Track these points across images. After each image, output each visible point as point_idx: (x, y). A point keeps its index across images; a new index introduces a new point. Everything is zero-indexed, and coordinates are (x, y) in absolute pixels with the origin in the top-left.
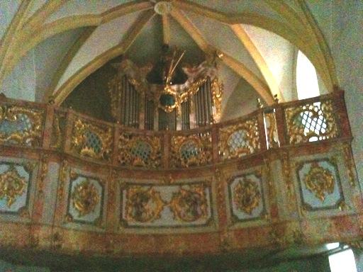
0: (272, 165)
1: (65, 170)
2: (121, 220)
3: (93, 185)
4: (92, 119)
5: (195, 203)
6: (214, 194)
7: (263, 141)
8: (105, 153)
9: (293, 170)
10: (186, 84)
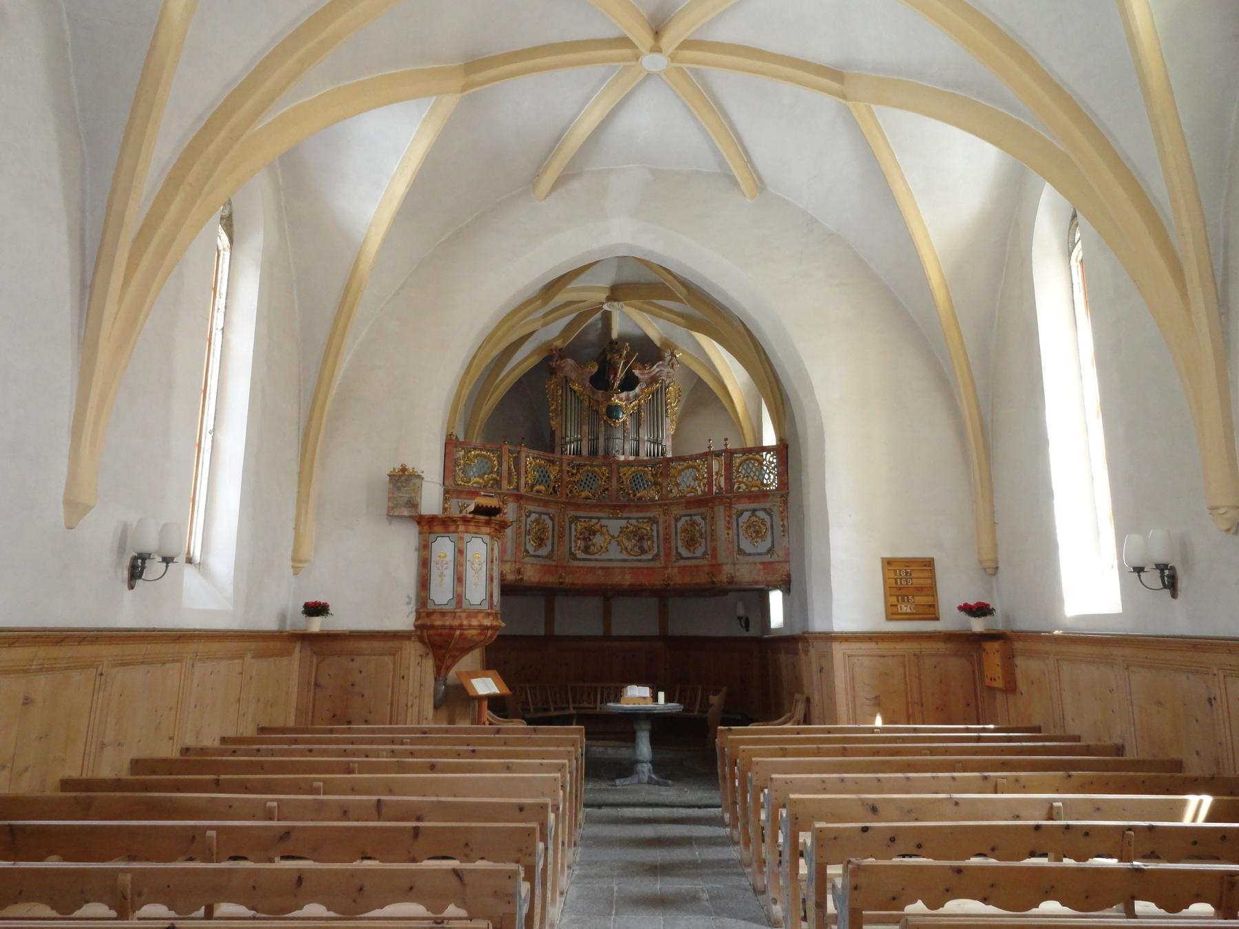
2: (571, 553)
5: (641, 539)
6: (661, 532)
7: (710, 484)
9: (734, 517)
10: (637, 390)
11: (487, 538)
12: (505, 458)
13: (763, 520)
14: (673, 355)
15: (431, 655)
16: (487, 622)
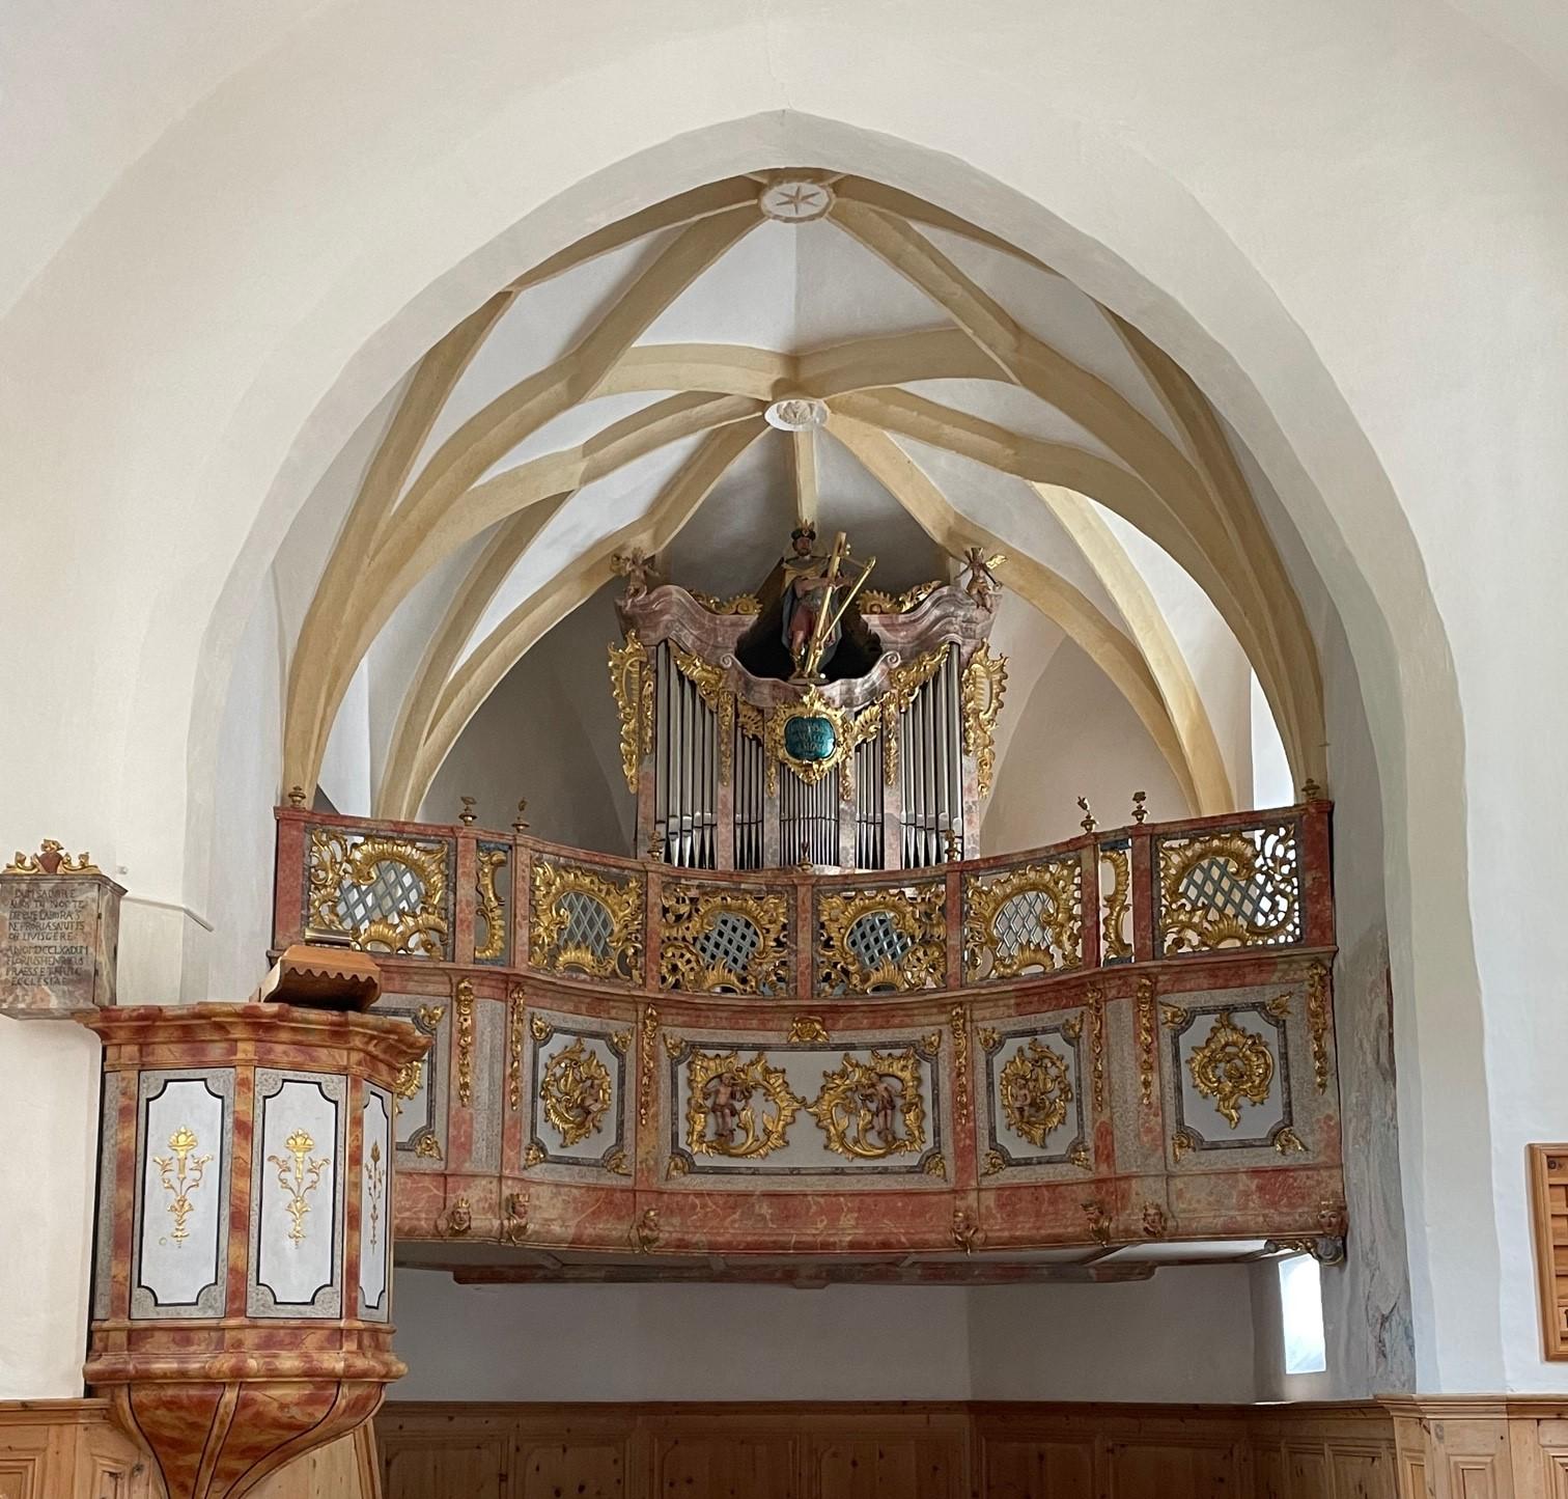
0: (1109, 1009)
1: (520, 1020)
2: (677, 1152)
3: (593, 1053)
4: (581, 853)
7: (1090, 935)
8: (623, 955)
9: (1166, 1032)
10: (876, 674)
11: (337, 1085)
12: (468, 863)
13: (1256, 1039)
14: (977, 564)
15: (149, 1463)
16: (334, 1362)
